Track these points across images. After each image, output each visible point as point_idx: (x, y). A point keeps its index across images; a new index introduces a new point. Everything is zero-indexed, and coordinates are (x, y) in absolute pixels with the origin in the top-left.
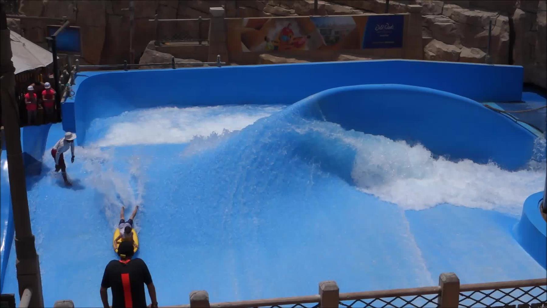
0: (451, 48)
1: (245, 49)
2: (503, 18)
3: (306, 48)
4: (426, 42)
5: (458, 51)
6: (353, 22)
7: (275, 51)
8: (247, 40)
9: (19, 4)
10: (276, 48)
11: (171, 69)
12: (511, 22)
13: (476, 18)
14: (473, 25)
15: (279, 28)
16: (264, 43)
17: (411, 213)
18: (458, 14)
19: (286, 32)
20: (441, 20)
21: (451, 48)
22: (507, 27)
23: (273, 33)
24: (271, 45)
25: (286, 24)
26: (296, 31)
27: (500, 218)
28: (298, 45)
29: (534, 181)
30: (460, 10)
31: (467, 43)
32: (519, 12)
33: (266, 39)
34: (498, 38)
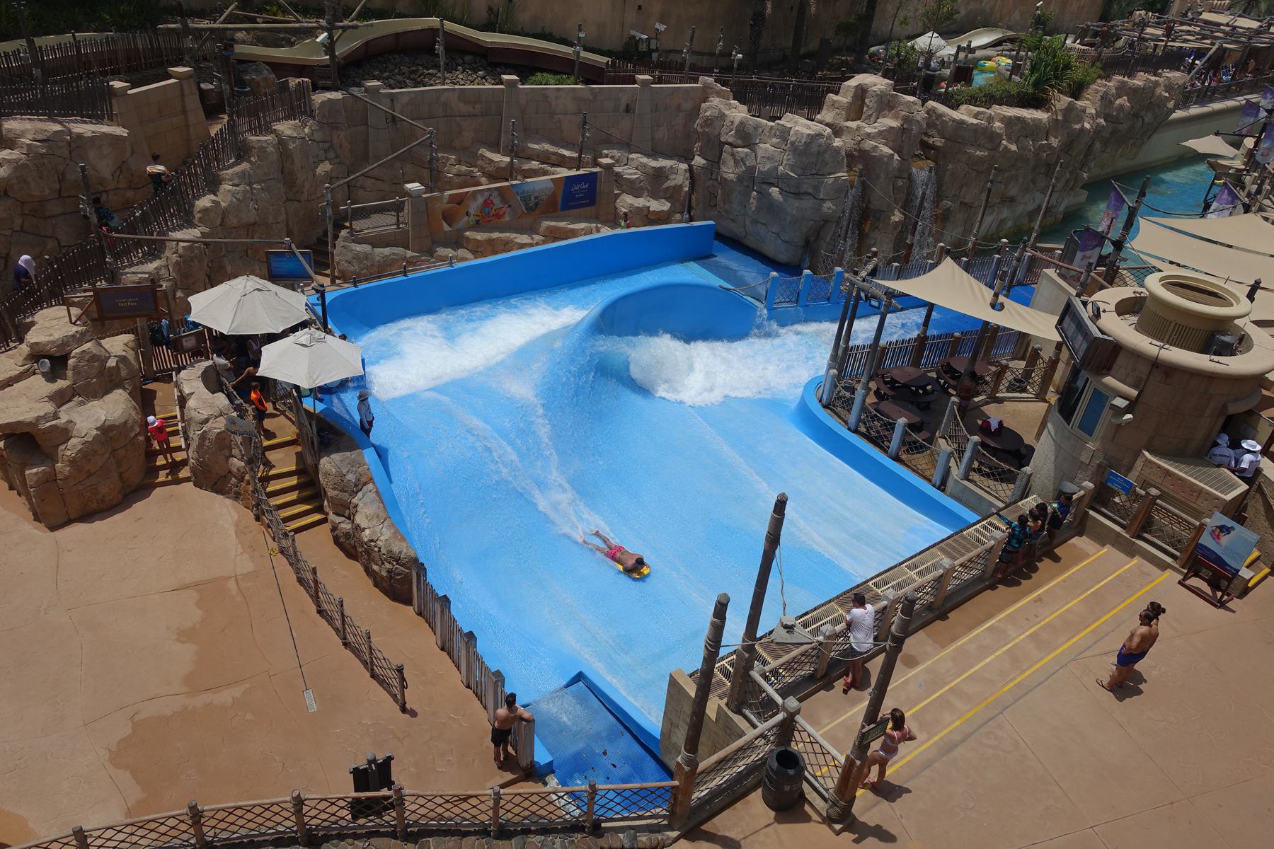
0: (640, 202)
1: (446, 228)
2: (684, 166)
3: (507, 218)
4: (617, 196)
5: (647, 204)
6: (551, 185)
7: (477, 226)
8: (448, 217)
9: (95, 104)
10: (478, 222)
11: (402, 278)
12: (691, 169)
13: (661, 168)
14: (659, 176)
15: (480, 200)
16: (466, 218)
17: (703, 411)
18: (645, 165)
19: (487, 203)
20: (629, 172)
21: (640, 202)
22: (688, 175)
23: (474, 207)
24: (472, 218)
25: (486, 194)
26: (497, 201)
27: (773, 404)
28: (498, 216)
29: (1019, 260)
30: (645, 160)
31: (655, 195)
32: (699, 161)
33: (467, 214)
34: (681, 187)
